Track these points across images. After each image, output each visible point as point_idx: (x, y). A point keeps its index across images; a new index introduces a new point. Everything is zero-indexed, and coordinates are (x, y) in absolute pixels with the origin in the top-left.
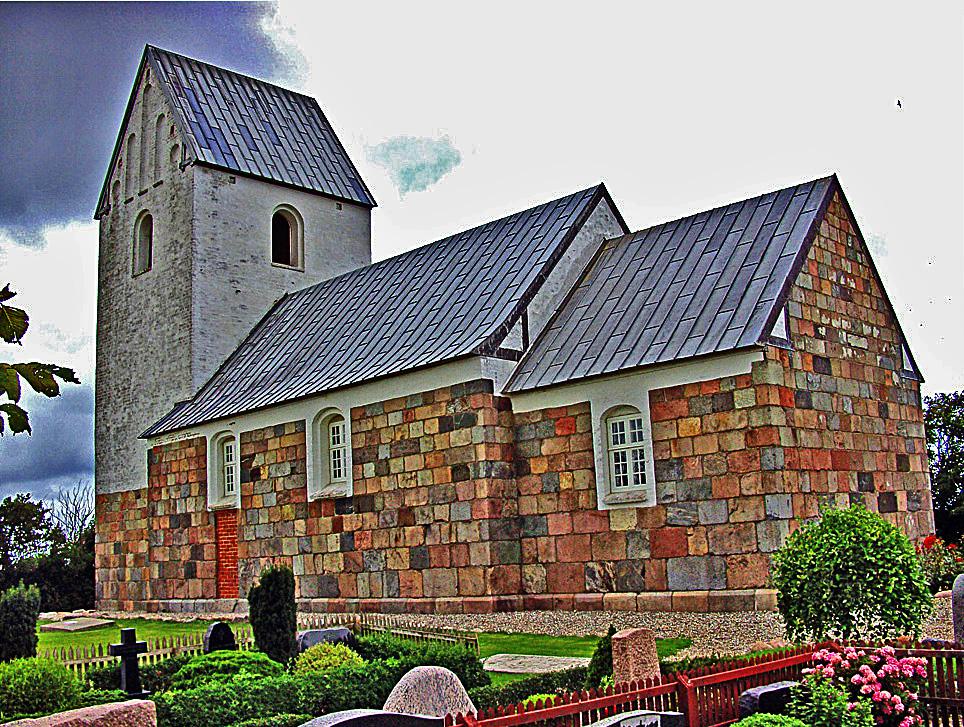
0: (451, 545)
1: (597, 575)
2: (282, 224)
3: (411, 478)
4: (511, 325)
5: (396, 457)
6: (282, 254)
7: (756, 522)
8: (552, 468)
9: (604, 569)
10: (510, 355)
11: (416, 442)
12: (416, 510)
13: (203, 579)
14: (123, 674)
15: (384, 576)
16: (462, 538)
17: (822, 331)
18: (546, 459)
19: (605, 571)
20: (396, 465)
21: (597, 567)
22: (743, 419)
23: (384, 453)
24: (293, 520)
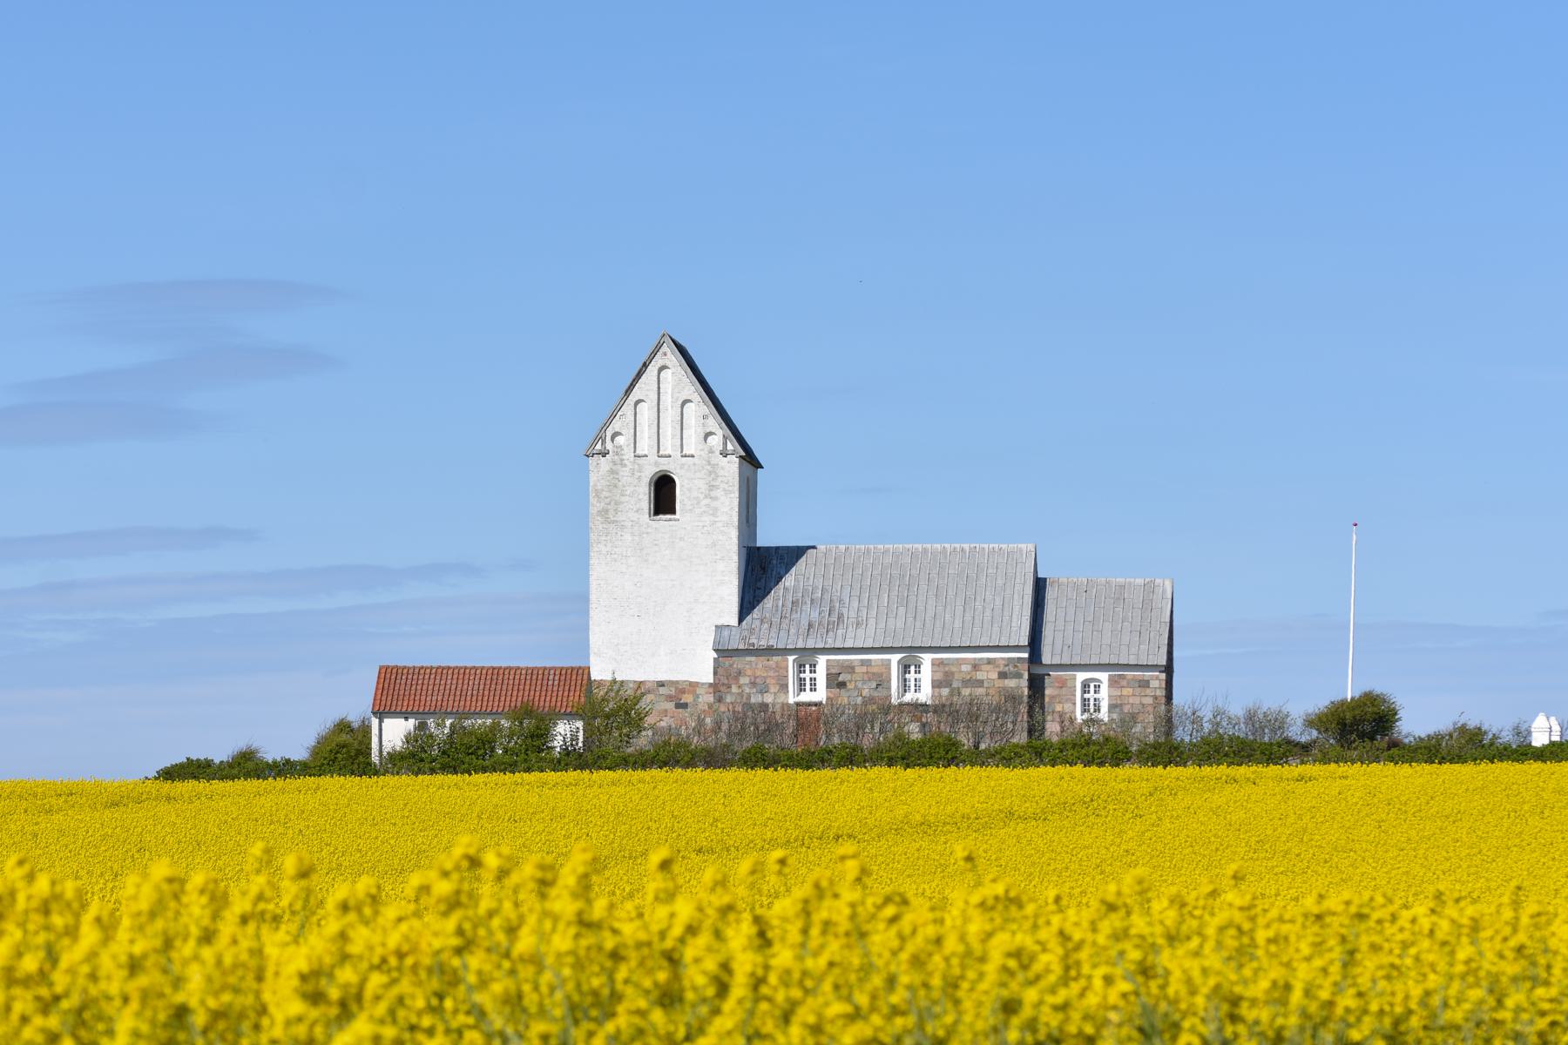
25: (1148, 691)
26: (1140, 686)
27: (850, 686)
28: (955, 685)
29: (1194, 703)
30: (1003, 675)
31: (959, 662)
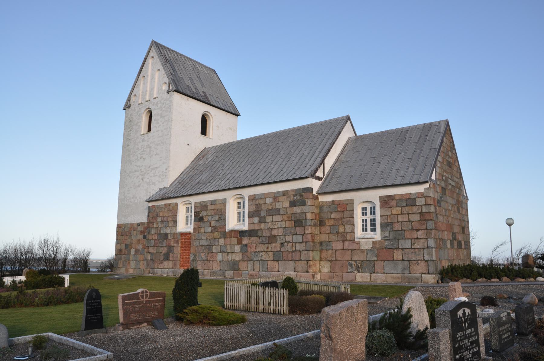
0: (293, 251)
1: (353, 266)
2: (204, 120)
3: (276, 224)
4: (319, 167)
5: (269, 216)
6: (204, 131)
7: (424, 249)
8: (335, 223)
9: (357, 264)
10: (319, 179)
11: (279, 210)
12: (277, 237)
13: (172, 261)
14: (139, 300)
15: (261, 263)
16: (298, 249)
17: (444, 178)
18: (333, 220)
19: (357, 264)
20: (269, 219)
21: (354, 263)
22: (419, 209)
23: (263, 214)
24: (219, 239)
25: (415, 209)
26: (407, 206)
27: (205, 219)
28: (262, 215)
29: (4, 245)
30: (293, 204)
31: (265, 196)
